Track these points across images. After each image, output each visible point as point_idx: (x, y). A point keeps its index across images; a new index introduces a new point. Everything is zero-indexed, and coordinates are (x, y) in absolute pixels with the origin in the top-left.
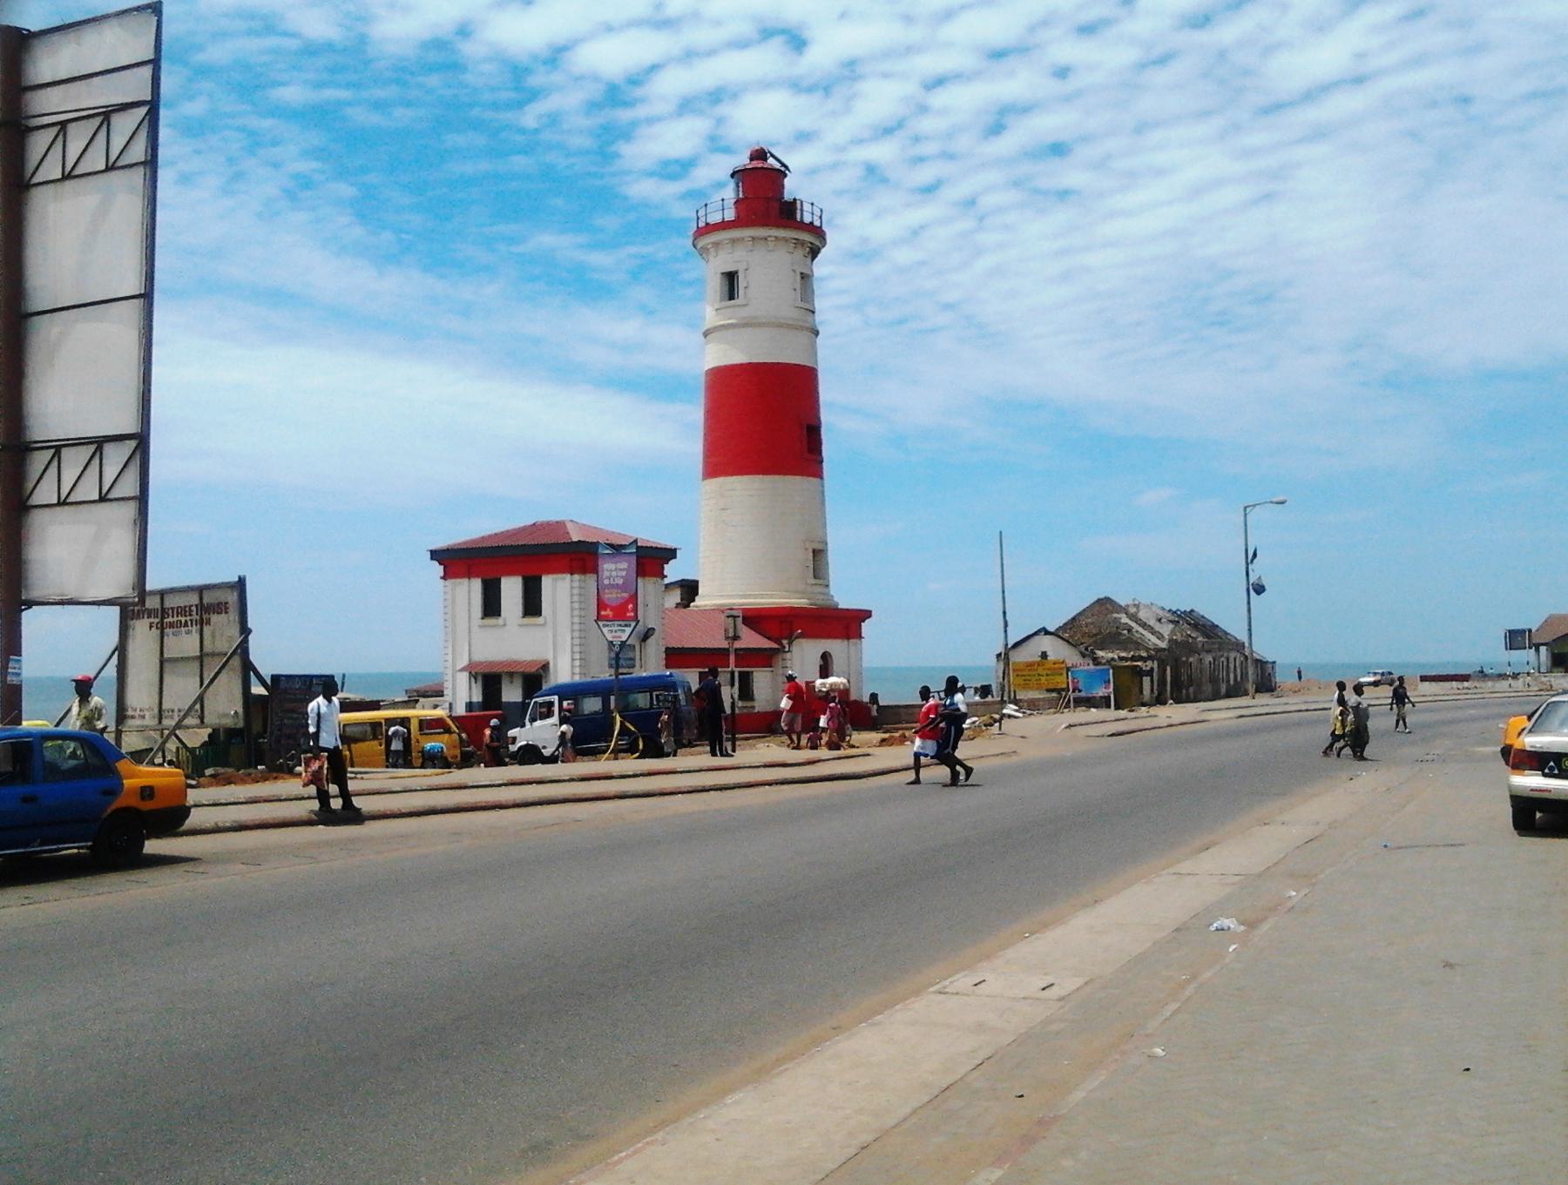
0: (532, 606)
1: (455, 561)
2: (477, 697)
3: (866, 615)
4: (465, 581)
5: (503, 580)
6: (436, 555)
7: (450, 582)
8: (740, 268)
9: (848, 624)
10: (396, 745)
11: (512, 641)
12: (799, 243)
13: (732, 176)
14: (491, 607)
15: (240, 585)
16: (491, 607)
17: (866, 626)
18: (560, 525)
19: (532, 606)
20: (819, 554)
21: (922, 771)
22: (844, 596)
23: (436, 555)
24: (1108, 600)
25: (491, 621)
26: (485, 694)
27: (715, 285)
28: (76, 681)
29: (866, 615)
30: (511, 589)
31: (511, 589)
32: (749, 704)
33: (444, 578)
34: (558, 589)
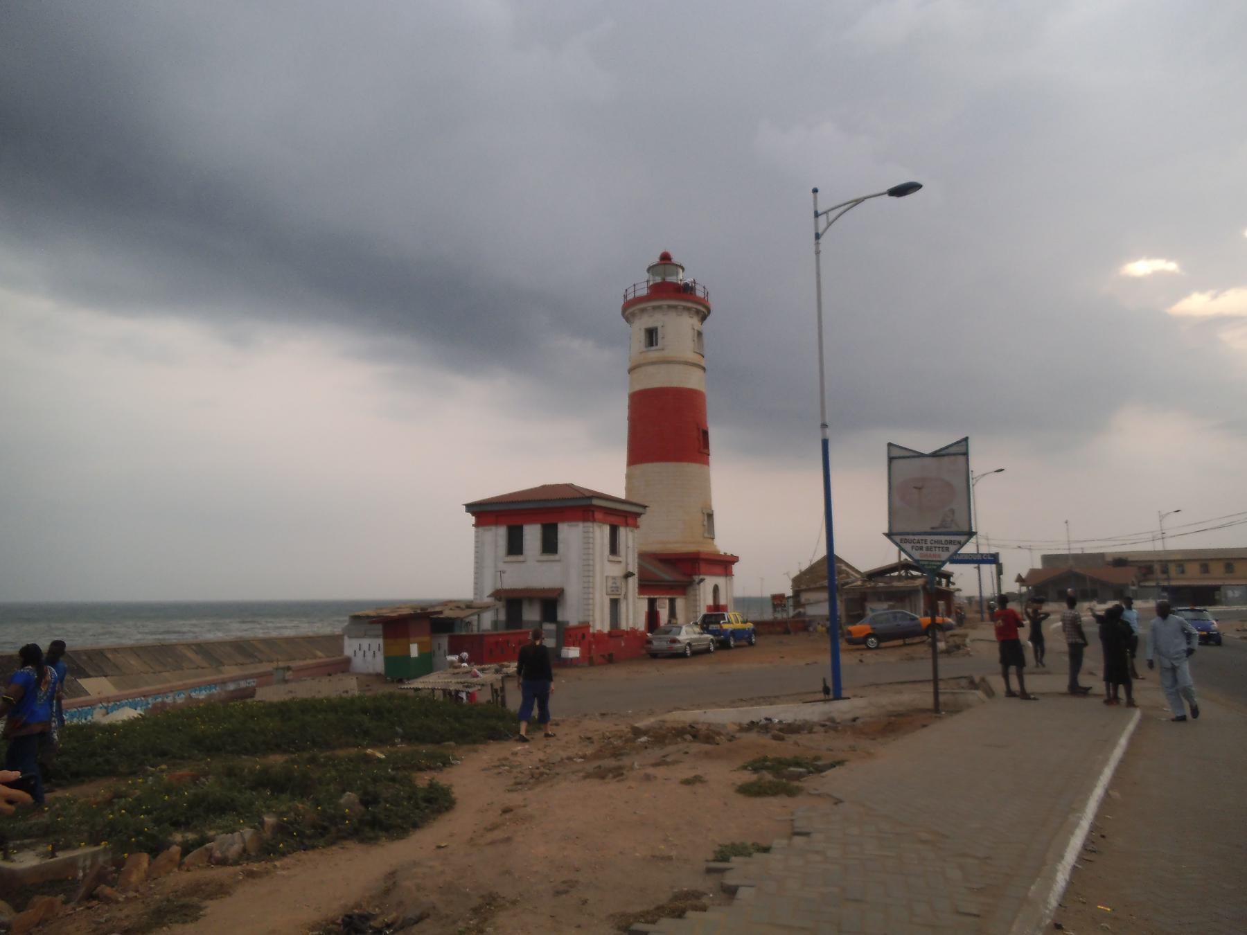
0: (550, 545)
1: (484, 513)
2: (502, 616)
3: (732, 560)
4: (493, 528)
6: (471, 508)
7: (481, 529)
8: (658, 324)
9: (725, 564)
10: (941, 604)
11: (533, 572)
12: (698, 312)
14: (515, 546)
15: (890, 445)
16: (515, 546)
17: (736, 568)
18: (570, 487)
20: (710, 516)
21: (943, 661)
22: (723, 544)
23: (471, 508)
26: (509, 614)
27: (642, 336)
29: (732, 560)
30: (532, 535)
31: (532, 535)
34: (569, 533)
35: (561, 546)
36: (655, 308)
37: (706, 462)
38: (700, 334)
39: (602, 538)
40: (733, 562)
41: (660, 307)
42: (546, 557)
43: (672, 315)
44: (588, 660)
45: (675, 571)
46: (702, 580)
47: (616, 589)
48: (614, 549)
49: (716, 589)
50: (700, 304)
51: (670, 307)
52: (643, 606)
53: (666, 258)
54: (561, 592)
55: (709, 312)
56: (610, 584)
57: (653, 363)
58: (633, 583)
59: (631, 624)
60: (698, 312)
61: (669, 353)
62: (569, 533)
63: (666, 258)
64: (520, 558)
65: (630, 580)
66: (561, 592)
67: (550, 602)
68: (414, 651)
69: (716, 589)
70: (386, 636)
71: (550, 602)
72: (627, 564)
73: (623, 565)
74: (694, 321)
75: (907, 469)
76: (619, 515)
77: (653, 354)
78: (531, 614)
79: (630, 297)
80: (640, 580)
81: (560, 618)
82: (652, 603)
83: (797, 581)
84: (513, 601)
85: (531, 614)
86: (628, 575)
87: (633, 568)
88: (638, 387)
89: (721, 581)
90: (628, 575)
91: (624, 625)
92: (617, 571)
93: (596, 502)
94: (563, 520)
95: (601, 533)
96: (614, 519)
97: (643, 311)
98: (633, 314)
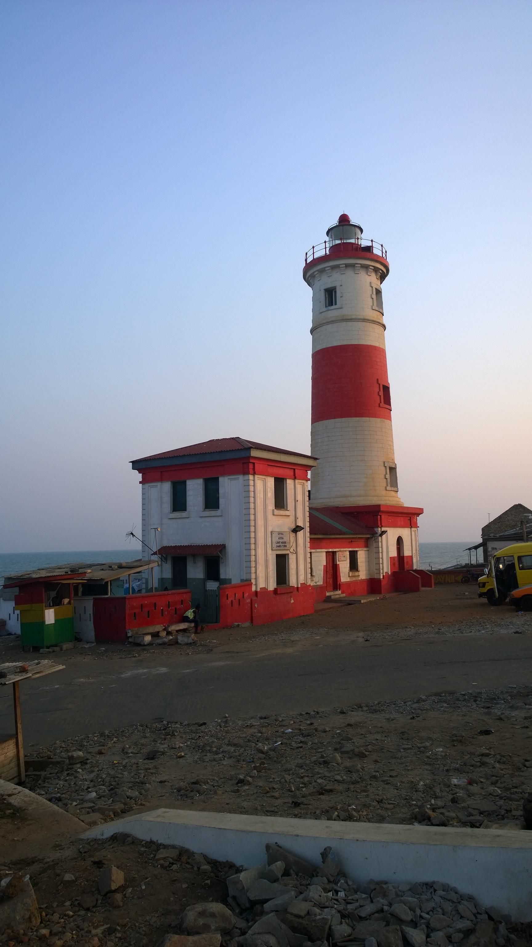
0: (212, 501)
1: (150, 469)
2: (168, 574)
3: (418, 512)
4: (159, 484)
5: (221, 479)
6: (137, 465)
7: (147, 485)
8: (337, 284)
9: (409, 517)
11: (196, 528)
12: (376, 270)
13: (328, 233)
14: (179, 503)
16: (179, 503)
17: (420, 520)
18: (236, 440)
19: (212, 501)
20: (393, 470)
22: (406, 497)
23: (137, 465)
24: (520, 506)
25: (177, 514)
28: (205, 508)
29: (418, 512)
30: (195, 489)
31: (195, 489)
32: (357, 574)
33: (140, 482)
35: (221, 501)
36: (333, 268)
37: (389, 418)
38: (379, 292)
39: (265, 492)
40: (418, 515)
41: (337, 267)
42: (208, 513)
43: (349, 273)
44: (522, 563)
45: (352, 522)
46: (384, 532)
47: (282, 544)
48: (280, 502)
49: (400, 541)
50: (377, 261)
51: (347, 266)
52: (320, 558)
53: (344, 220)
54: (222, 548)
55: (388, 271)
56: (276, 539)
57: (333, 322)
58: (303, 537)
59: (302, 580)
60: (376, 270)
61: (346, 312)
62: (228, 485)
63: (344, 220)
64: (184, 514)
65: (300, 534)
66: (222, 548)
67: (213, 558)
68: (50, 616)
69: (400, 541)
70: (19, 601)
71: (213, 558)
72: (296, 518)
73: (292, 518)
74: (373, 278)
75: (395, 489)
76: (283, 467)
77: (333, 313)
78: (196, 571)
79: (310, 260)
80: (311, 533)
81: (222, 577)
82: (332, 557)
83: (486, 530)
84: (177, 557)
85: (196, 571)
86: (297, 529)
87: (303, 520)
88: (319, 348)
89: (405, 533)
90: (297, 529)
91: (472, 563)
92: (288, 524)
93: (254, 453)
94: (224, 474)
95: (262, 487)
96: (281, 472)
97: (322, 271)
98: (313, 276)
